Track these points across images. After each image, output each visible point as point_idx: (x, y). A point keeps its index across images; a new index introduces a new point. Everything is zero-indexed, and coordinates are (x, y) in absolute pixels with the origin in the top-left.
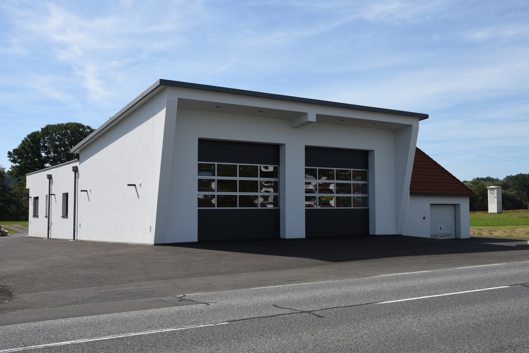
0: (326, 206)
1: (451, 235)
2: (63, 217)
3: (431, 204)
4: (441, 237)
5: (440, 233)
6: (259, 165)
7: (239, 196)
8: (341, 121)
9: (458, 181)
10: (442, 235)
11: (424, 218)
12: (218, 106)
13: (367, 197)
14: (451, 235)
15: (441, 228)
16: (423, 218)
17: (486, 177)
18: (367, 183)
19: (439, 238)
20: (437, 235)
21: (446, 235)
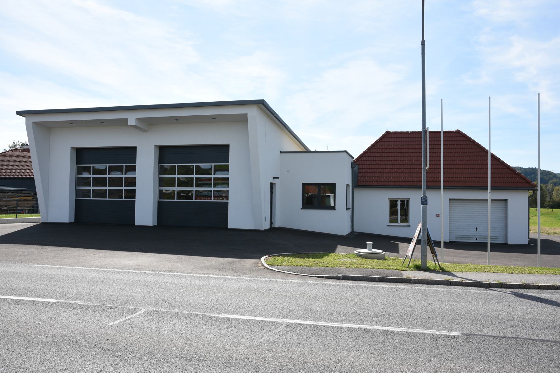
0: (218, 199)
1: (496, 239)
3: (450, 200)
4: (476, 239)
7: (108, 189)
8: (71, 124)
9: (507, 167)
10: (479, 237)
11: (438, 215)
12: (72, 123)
14: (496, 239)
15: (477, 229)
18: (77, 175)
20: (470, 237)
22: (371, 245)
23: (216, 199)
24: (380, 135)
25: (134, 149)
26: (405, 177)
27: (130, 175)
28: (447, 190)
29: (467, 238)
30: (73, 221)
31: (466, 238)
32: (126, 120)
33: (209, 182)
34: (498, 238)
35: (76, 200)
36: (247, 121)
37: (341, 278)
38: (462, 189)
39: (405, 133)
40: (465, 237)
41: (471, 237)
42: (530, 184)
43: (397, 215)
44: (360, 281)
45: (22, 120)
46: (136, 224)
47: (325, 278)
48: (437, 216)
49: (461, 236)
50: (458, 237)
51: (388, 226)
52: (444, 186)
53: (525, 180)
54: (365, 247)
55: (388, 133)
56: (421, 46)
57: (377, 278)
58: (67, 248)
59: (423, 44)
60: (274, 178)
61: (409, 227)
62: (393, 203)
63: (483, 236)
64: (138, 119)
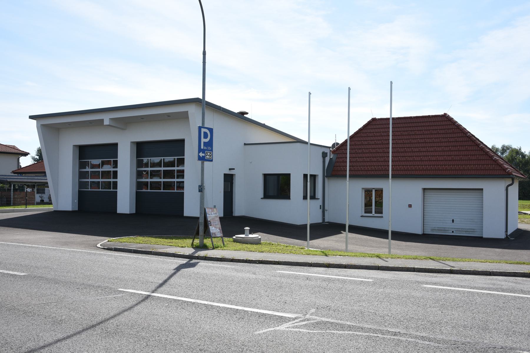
1: (473, 232)
2: (245, 143)
4: (453, 232)
5: (451, 227)
6: (90, 160)
12: (70, 124)
13: (138, 168)
14: (473, 232)
15: (453, 221)
16: (412, 206)
17: (367, 122)
19: (450, 233)
20: (446, 229)
21: (463, 230)
22: (248, 231)
23: (178, 189)
24: (365, 122)
25: (116, 145)
26: (484, 165)
27: (180, 168)
28: (367, 178)
29: (443, 230)
30: (77, 209)
31: (442, 230)
32: (102, 121)
33: (182, 174)
34: (475, 231)
35: (137, 192)
36: (188, 118)
37: (113, 250)
38: (455, 178)
39: (427, 117)
40: (441, 229)
41: (447, 229)
42: (506, 171)
43: (371, 206)
44: (123, 252)
45: (34, 122)
46: (118, 212)
47: (106, 249)
48: (409, 207)
49: (436, 229)
50: (434, 230)
51: (361, 217)
52: (392, 175)
53: (501, 167)
54: (243, 233)
55: (374, 120)
56: (202, 55)
57: (153, 252)
58: (14, 229)
59: (204, 53)
60: (230, 169)
61: (382, 218)
62: (368, 192)
63: (460, 229)
64: (111, 119)
